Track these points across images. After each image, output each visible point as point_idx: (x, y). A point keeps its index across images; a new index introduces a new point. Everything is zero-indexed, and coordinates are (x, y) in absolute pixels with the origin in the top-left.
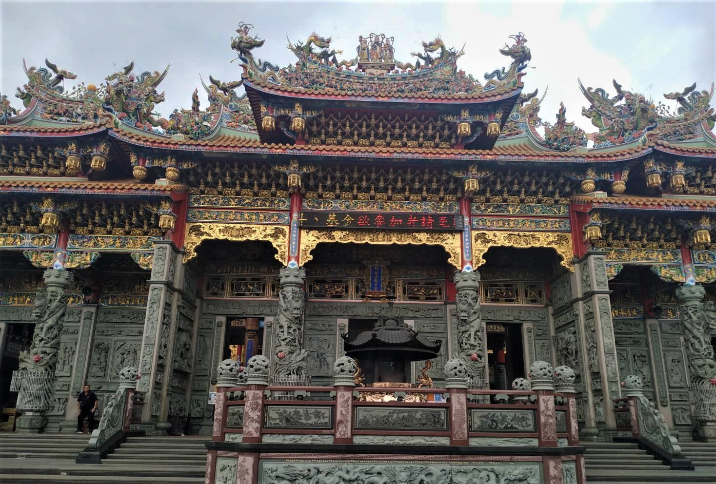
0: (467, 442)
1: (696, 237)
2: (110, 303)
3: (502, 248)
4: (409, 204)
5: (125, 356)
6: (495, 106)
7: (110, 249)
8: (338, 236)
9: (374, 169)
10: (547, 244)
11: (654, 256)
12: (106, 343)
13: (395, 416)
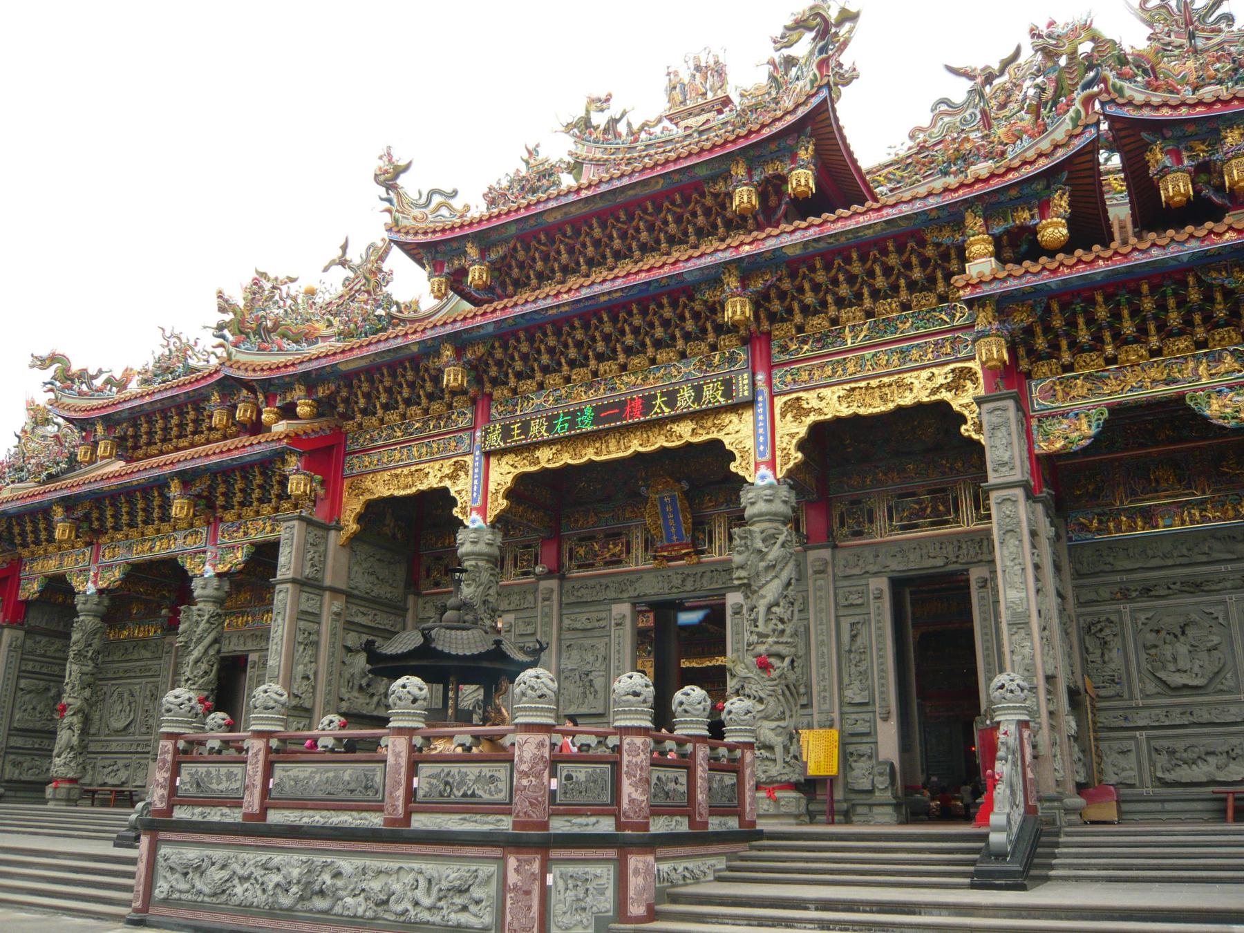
3: (838, 421)
4: (659, 369)
8: (547, 458)
9: (891, 246)
11: (1188, 372)
13: (317, 777)
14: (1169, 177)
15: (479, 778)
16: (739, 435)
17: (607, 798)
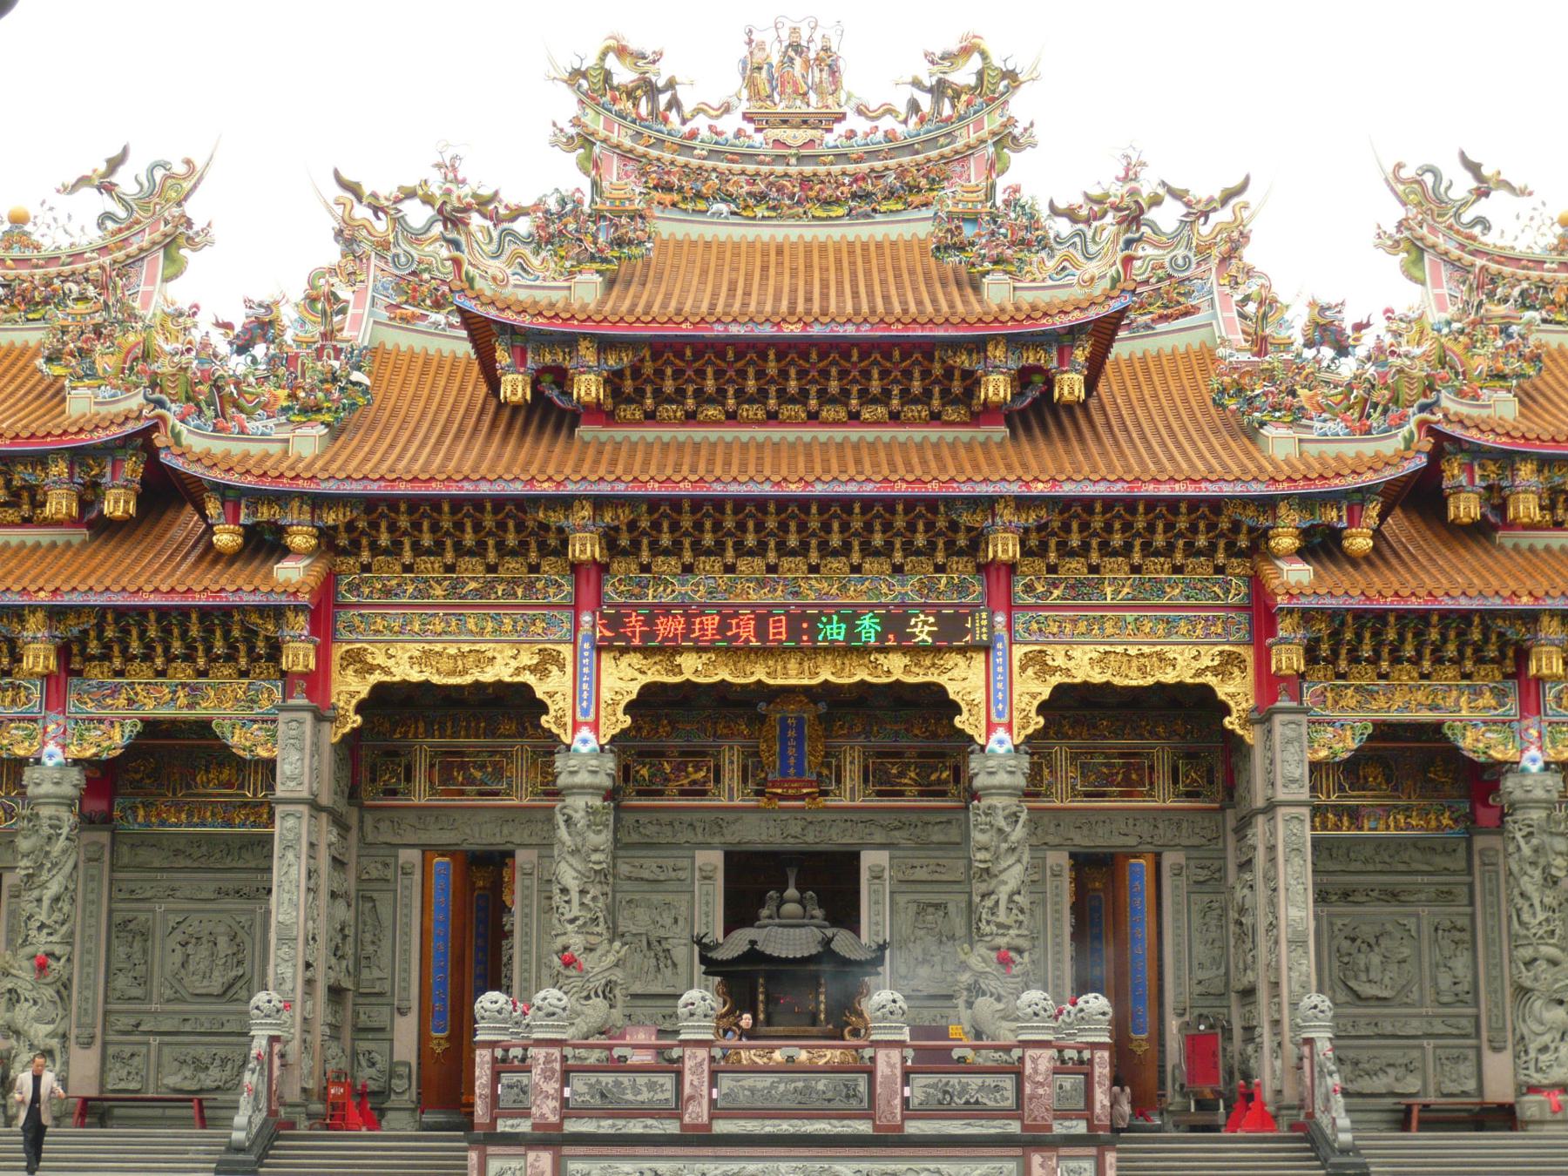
0: (901, 1127)
1: (1539, 660)
2: (140, 819)
4: (862, 581)
5: (190, 949)
7: (165, 712)
8: (692, 668)
10: (1195, 675)
11: (1450, 702)
12: (142, 917)
13: (782, 1087)
14: (1462, 496)
15: (981, 1088)
16: (964, 684)
17: (1082, 1105)
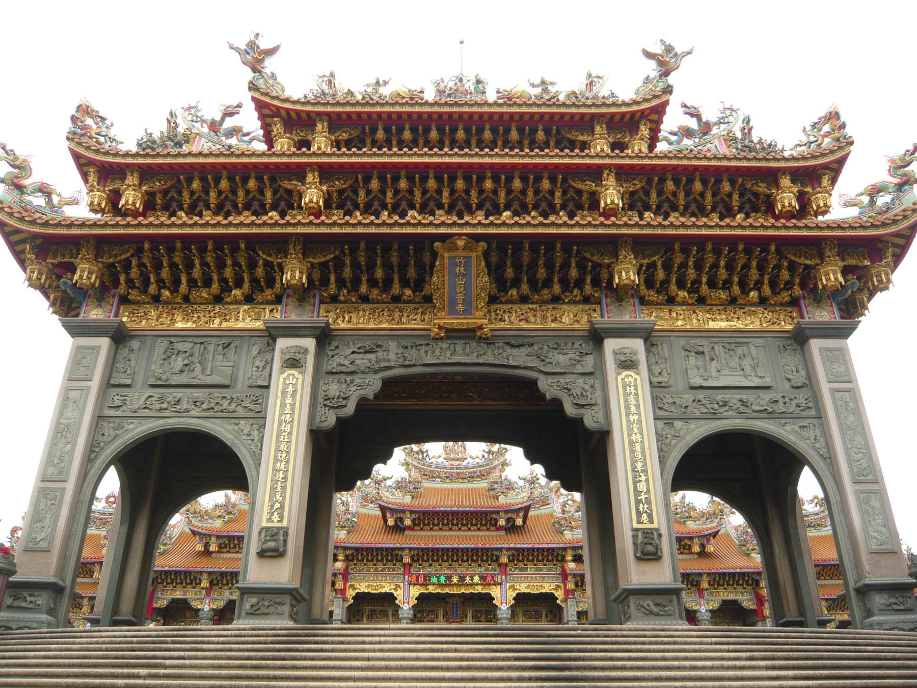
6: (520, 509)
8: (431, 589)
